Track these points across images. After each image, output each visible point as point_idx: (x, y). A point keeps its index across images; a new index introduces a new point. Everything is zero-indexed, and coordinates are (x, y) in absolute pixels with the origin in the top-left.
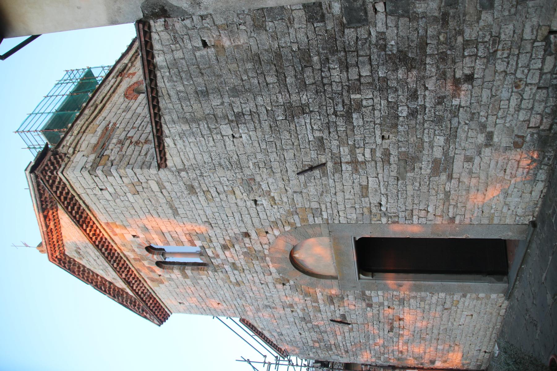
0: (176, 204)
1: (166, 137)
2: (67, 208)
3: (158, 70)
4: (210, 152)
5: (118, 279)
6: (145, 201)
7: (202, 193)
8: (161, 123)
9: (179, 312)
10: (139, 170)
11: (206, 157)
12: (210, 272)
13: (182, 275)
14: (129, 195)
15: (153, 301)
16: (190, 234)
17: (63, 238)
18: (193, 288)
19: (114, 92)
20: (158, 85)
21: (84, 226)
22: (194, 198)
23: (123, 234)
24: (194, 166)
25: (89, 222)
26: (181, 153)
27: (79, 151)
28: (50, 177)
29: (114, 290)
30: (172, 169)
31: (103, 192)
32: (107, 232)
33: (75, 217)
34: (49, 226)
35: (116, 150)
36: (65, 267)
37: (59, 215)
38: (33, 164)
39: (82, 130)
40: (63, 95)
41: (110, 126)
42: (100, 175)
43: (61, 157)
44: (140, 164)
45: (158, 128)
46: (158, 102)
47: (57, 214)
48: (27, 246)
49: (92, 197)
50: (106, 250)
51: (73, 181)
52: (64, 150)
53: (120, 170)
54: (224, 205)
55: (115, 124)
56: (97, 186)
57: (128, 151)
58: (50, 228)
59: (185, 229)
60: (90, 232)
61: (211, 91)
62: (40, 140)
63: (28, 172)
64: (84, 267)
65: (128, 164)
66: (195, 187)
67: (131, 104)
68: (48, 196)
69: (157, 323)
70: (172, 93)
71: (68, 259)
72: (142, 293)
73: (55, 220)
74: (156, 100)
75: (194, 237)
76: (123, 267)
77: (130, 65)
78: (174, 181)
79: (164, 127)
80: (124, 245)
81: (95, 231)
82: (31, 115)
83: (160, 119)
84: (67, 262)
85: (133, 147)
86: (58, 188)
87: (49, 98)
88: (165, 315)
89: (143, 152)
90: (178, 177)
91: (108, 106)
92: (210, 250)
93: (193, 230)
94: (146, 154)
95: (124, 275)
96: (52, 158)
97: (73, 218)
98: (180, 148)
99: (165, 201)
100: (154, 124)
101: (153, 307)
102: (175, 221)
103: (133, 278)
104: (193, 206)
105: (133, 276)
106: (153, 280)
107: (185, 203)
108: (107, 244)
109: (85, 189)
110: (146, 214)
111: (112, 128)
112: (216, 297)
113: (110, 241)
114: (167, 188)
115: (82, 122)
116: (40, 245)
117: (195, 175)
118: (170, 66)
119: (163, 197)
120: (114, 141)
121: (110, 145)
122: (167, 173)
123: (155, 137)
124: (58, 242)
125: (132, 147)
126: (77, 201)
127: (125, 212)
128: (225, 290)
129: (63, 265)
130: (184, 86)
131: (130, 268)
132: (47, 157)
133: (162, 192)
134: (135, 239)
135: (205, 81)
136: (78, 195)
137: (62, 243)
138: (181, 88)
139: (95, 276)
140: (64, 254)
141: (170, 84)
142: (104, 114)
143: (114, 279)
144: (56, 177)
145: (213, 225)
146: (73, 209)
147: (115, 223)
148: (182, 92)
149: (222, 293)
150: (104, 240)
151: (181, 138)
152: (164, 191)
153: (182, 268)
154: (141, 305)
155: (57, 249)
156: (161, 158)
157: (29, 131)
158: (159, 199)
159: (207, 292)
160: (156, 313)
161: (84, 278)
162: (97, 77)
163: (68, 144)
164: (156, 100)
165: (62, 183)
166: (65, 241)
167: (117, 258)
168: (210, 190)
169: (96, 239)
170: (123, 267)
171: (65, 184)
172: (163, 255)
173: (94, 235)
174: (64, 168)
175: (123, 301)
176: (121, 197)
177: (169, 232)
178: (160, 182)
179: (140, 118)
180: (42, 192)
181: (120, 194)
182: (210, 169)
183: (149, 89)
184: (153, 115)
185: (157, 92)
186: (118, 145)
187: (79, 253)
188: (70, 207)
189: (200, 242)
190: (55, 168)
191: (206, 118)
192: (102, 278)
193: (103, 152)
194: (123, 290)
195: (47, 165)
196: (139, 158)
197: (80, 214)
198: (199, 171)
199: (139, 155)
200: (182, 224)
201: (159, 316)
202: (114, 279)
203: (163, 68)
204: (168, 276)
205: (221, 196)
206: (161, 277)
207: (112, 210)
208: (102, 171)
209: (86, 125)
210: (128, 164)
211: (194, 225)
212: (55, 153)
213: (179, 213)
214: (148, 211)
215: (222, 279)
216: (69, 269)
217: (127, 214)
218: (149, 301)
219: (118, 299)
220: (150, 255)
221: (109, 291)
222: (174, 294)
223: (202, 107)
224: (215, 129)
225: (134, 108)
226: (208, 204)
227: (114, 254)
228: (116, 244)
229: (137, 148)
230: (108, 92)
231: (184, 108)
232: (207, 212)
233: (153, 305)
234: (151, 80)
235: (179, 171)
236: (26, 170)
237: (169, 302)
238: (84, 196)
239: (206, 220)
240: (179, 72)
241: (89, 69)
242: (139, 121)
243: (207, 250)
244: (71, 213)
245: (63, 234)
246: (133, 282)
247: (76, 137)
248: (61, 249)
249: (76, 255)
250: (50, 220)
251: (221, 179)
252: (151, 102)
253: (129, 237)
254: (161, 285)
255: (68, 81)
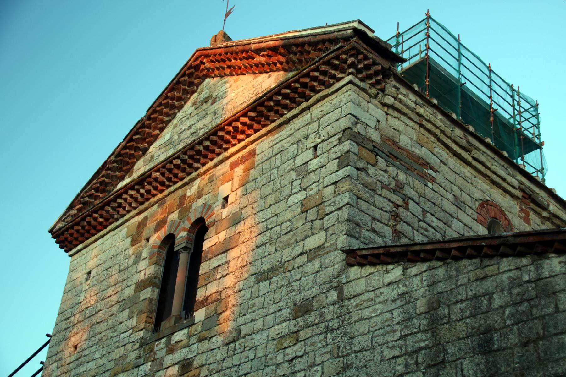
0: (277, 280)
1: (404, 269)
2: (288, 87)
3: (534, 261)
4: (371, 348)
5: (152, 165)
6: (288, 224)
7: (295, 329)
8: (430, 260)
9: (72, 270)
10: (346, 216)
11: (363, 341)
12: (141, 334)
13: (142, 281)
14: (302, 196)
15: (101, 223)
16: (219, 300)
17: (235, 77)
18: (114, 298)
19: (493, 182)
20: (504, 259)
21: (252, 114)
22: (286, 312)
23: (232, 179)
24: (347, 317)
25: (259, 122)
26: (372, 295)
27: (387, 114)
28: (345, 61)
29: (131, 156)
30: (344, 276)
31: (311, 151)
32: (238, 152)
33: (270, 99)
34: (258, 54)
35: (385, 178)
36: (182, 76)
37: (276, 74)
38: (370, 34)
39: (424, 123)
40: (490, 98)
41: (430, 171)
42: (340, 147)
43: (378, 82)
44: (356, 219)
45: (422, 255)
46: (470, 257)
47: (278, 70)
48: (227, 16)
49: (304, 131)
50: (207, 148)
51: (335, 99)
52: (390, 89)
53: (348, 183)
54: (268, 370)
55: (433, 180)
56: (323, 141)
57: (382, 199)
58: (255, 55)
59: (230, 292)
60: (242, 123)
61: (491, 359)
62: (412, 55)
63: (356, 25)
64: (180, 108)
65: (358, 198)
66: (307, 316)
67: (470, 211)
68: (311, 56)
69: (57, 228)
70: (488, 285)
71: (196, 81)
72: (120, 205)
73: (269, 65)
74: (474, 253)
75: (212, 307)
76: (171, 176)
77: (545, 214)
78: (322, 277)
79: (424, 266)
80: (211, 181)
81: (243, 132)
82: (458, 41)
83: (438, 259)
84: (192, 79)
85: (388, 208)
86: (324, 73)
87: (488, 73)
88: (71, 242)
89: (378, 226)
90: (328, 286)
91: (467, 171)
92: (184, 338)
93: (227, 307)
94: (374, 231)
95: (157, 175)
96: (379, 68)
97: (269, 95)
98: (382, 293)
99: (285, 259)
100: (429, 247)
101: (89, 223)
102: (246, 275)
103: (148, 192)
104: (272, 311)
105: (154, 192)
106: (141, 225)
107: (278, 295)
108: (217, 150)
109: (319, 119)
110: (265, 224)
111: (426, 174)
112: (91, 344)
113: (221, 157)
114: (310, 264)
115: (439, 123)
116: (226, 37)
117: (329, 317)
118: (541, 283)
119: (293, 255)
120: (402, 177)
121: (395, 169)
122: (337, 266)
123: (405, 248)
124: (229, 67)
125: (389, 207)
126: (299, 104)
127: (271, 187)
128: (101, 362)
129: (188, 72)
130: (501, 307)
131: (168, 187)
132: (379, 60)
133: (302, 254)
134: (222, 201)
135: (511, 348)
136: (308, 108)
137: (226, 75)
138: (497, 302)
139: (160, 126)
140: (206, 76)
141: (507, 281)
142: (452, 161)
143: (152, 157)
144: (343, 71)
145: (232, 345)
146: (285, 96)
147: (253, 167)
148: (490, 304)
149: (97, 355)
150: (224, 146)
151: (401, 296)
152: (304, 258)
153: (156, 281)
154: (97, 202)
155: (217, 64)
156: (364, 257)
157: (428, 36)
158: (290, 249)
159: (103, 326)
160: (76, 228)
161: (158, 106)
162: (523, 159)
163: (400, 96)
164: (474, 253)
165: (332, 81)
166: (231, 79)
167: (190, 166)
168: (299, 344)
169: (228, 133)
170: (171, 176)
171: (330, 85)
172: (185, 248)
173: (236, 129)
174: (358, 87)
175: (108, 169)
176: (298, 182)
177: (227, 263)
178: (320, 253)
179: (441, 225)
180: (319, 47)
181: (305, 180)
182: (339, 347)
183: (497, 242)
184: (446, 246)
185: (491, 257)
186: (393, 183)
187: (206, 100)
188: (288, 91)
189: (203, 319)
190: (359, 71)
191: (438, 345)
192: (156, 137)
193: (384, 155)
194: (129, 171)
195: (366, 58)
196: (368, 218)
197: (276, 108)
198: (336, 325)
199: (374, 219)
200: (239, 286)
201: (71, 231)
202: (152, 157)
203: (537, 269)
204: (144, 255)
205: (286, 365)
206: (144, 242)
207: (278, 164)
208: (348, 152)
209: (434, 129)
210: (358, 198)
211: (236, 309)
212: (387, 74)
213: (261, 284)
214: (269, 227)
215: (124, 357)
216: (178, 82)
217: (267, 190)
218: (102, 216)
219: (114, 162)
220: (187, 225)
221: (131, 148)
222: (109, 263)
223: (460, 339)
224: (417, 363)
225: (462, 215)
226: (273, 339)
227: (198, 161)
228: (216, 166)
229: (387, 216)
230: (494, 173)
231: (459, 305)
232: (257, 337)
233: (93, 222)
234: (513, 247)
235: (339, 288)
236: (360, 22)
237: (95, 252)
238: (307, 117)
239: (243, 333)
240: (529, 300)
241: (539, 146)
242: (436, 223)
243: (185, 331)
244: (279, 93)
245: (241, 77)
246: (142, 191)
247: (413, 110)
248: (216, 72)
249: (203, 96)
250: (269, 56)
251: (319, 368)
252: (470, 243)
253: (225, 189)
254: (129, 240)
255: (517, 107)
